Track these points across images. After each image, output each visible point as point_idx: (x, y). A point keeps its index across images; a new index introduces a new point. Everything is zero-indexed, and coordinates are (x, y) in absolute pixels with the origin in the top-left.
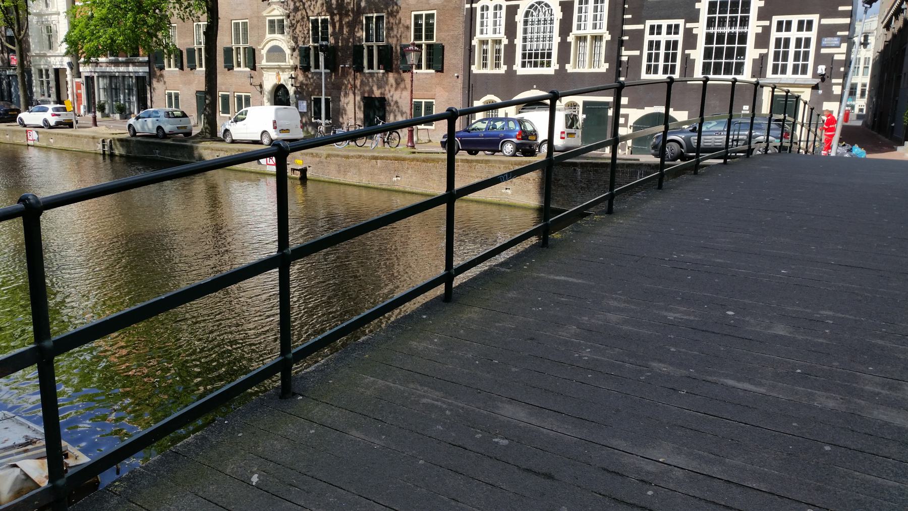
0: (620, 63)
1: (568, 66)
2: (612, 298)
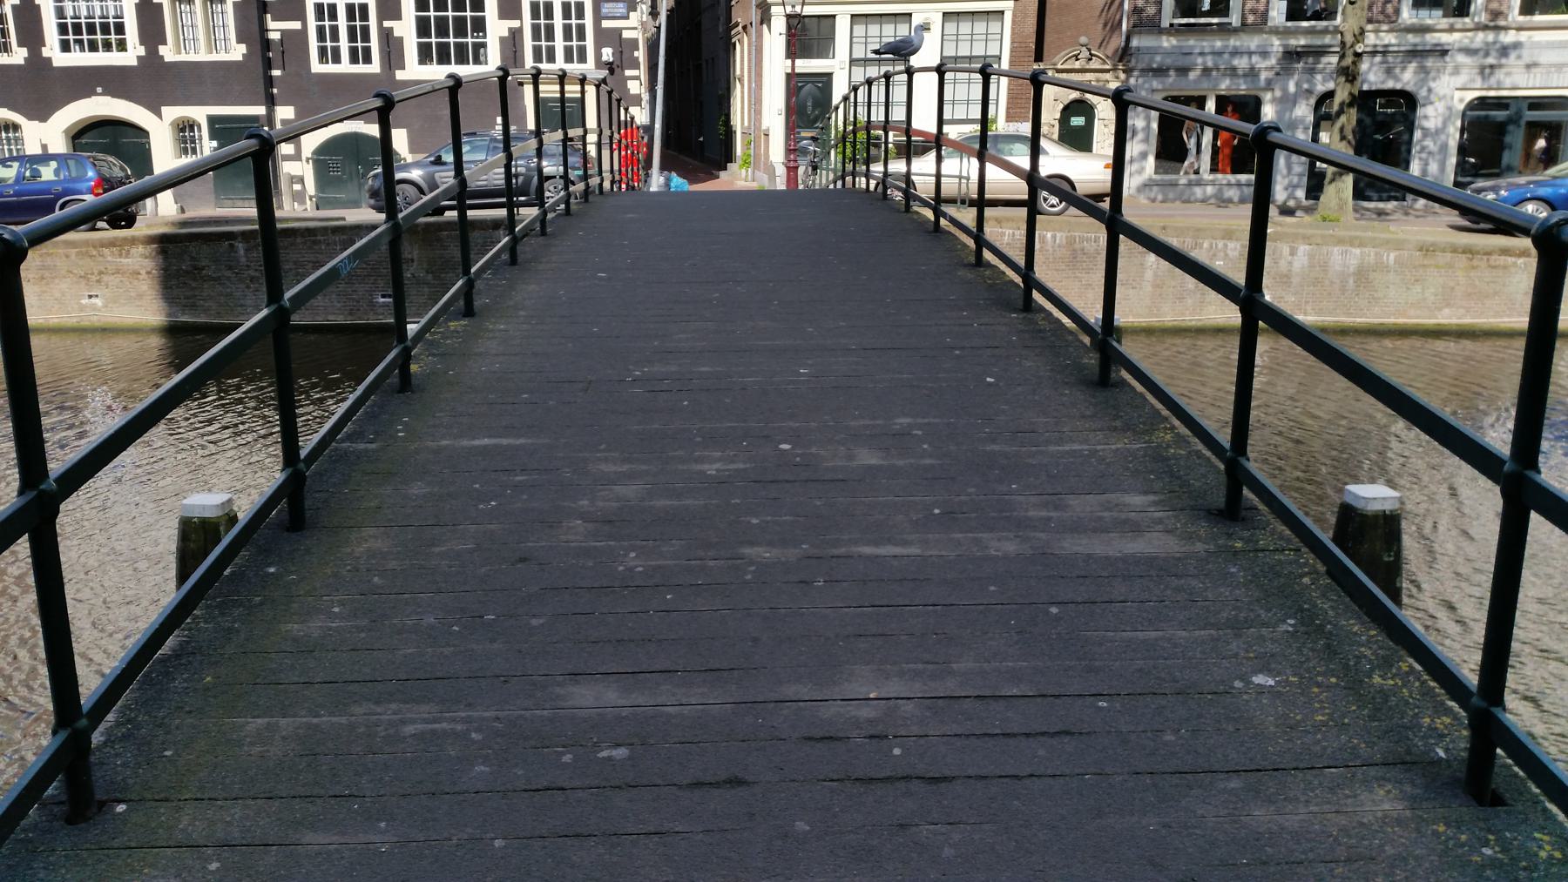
0: (266, 44)
1: (162, 50)
2: (599, 459)
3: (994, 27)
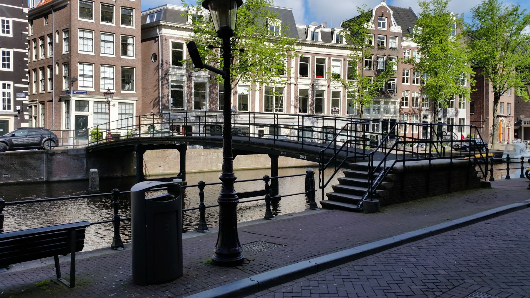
3: (131, 107)
